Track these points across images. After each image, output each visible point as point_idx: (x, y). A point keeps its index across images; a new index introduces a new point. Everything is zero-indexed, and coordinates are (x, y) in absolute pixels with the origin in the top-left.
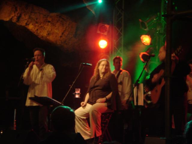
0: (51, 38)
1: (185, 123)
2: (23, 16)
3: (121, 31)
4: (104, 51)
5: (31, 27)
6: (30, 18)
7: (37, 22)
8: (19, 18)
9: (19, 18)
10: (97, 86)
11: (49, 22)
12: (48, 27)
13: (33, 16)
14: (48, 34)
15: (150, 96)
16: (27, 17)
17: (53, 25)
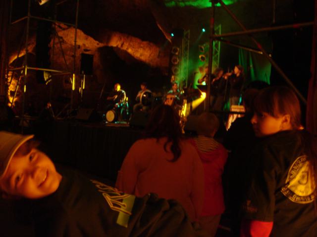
0: (143, 58)
1: (227, 119)
2: (125, 43)
3: (18, 179)
4: (212, 98)
5: (130, 51)
6: (129, 44)
7: (133, 48)
8: (122, 45)
9: (122, 45)
10: (67, 25)
11: (141, 47)
12: (141, 51)
13: (131, 44)
14: (141, 55)
15: (50, 48)
16: (127, 44)
17: (144, 49)
